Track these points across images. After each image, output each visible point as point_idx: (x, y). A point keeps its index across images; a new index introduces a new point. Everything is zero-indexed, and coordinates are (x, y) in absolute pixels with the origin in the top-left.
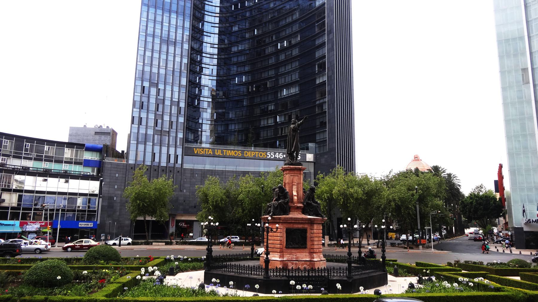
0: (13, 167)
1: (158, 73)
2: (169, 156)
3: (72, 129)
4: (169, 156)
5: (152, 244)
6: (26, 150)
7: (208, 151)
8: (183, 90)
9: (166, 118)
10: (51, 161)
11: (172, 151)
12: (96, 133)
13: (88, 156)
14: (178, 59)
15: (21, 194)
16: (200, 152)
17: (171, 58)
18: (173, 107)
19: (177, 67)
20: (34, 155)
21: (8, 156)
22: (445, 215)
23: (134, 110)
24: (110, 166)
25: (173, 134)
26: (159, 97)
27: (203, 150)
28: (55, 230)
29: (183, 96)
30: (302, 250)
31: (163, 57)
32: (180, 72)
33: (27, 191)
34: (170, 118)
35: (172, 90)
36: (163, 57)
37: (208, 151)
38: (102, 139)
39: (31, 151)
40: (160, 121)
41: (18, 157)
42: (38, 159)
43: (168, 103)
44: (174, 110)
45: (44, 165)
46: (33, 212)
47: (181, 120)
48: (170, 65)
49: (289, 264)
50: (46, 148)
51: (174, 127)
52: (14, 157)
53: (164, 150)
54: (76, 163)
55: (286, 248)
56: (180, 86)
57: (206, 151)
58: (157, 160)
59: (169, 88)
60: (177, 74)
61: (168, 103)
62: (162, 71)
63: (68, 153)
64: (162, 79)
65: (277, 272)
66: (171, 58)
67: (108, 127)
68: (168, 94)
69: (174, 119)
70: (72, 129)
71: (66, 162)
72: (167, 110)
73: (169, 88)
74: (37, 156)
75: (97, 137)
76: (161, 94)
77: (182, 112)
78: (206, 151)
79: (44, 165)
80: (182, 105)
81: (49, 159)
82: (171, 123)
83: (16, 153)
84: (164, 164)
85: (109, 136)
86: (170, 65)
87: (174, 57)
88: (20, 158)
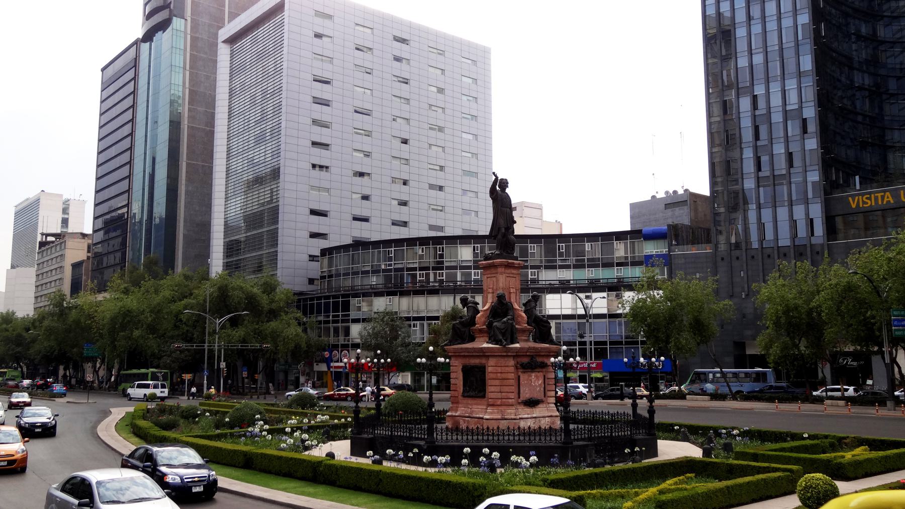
0: (548, 283)
1: (751, 66)
2: (793, 224)
3: (633, 206)
4: (793, 224)
5: (685, 398)
6: (561, 255)
7: (883, 197)
8: (809, 84)
9: (779, 149)
10: (597, 266)
11: (799, 212)
12: (667, 206)
13: (651, 248)
14: (787, 22)
15: (558, 321)
16: (864, 202)
17: (772, 26)
18: (789, 123)
19: (788, 38)
20: (572, 260)
21: (538, 267)
22: (777, 324)
23: (715, 150)
24: (683, 261)
25: (796, 179)
26: (757, 112)
27: (869, 199)
28: (211, 364)
29: (810, 94)
30: (478, 401)
31: (757, 29)
32: (797, 45)
33: (566, 317)
34: (787, 148)
35: (784, 92)
36: (757, 29)
37: (883, 197)
38: (677, 213)
39: (568, 254)
40: (765, 159)
41: (551, 267)
42: (579, 266)
43: (777, 118)
44: (794, 129)
45: (588, 274)
46: (577, 347)
47: (812, 143)
48: (773, 40)
49: (461, 422)
50: (588, 246)
51: (797, 162)
52: (547, 267)
53: (783, 213)
54: (635, 264)
55: (463, 396)
56: (800, 74)
57: (876, 198)
58: (769, 235)
59: (775, 88)
60: (789, 54)
61: (777, 118)
62: (758, 59)
63: (620, 250)
64: (759, 74)
65: (478, 435)
66: (772, 26)
67: (667, 192)
68: (776, 100)
69: (794, 148)
70: (633, 206)
71: (619, 264)
72: (779, 132)
73: (775, 88)
74: (577, 260)
75: (669, 212)
76: (762, 104)
77: (812, 127)
78: (876, 198)
79: (588, 274)
80: (810, 112)
81: (593, 264)
82: (790, 156)
83: (548, 261)
84: (785, 241)
85: (686, 207)
86: (773, 40)
87: (779, 19)
88: (554, 267)
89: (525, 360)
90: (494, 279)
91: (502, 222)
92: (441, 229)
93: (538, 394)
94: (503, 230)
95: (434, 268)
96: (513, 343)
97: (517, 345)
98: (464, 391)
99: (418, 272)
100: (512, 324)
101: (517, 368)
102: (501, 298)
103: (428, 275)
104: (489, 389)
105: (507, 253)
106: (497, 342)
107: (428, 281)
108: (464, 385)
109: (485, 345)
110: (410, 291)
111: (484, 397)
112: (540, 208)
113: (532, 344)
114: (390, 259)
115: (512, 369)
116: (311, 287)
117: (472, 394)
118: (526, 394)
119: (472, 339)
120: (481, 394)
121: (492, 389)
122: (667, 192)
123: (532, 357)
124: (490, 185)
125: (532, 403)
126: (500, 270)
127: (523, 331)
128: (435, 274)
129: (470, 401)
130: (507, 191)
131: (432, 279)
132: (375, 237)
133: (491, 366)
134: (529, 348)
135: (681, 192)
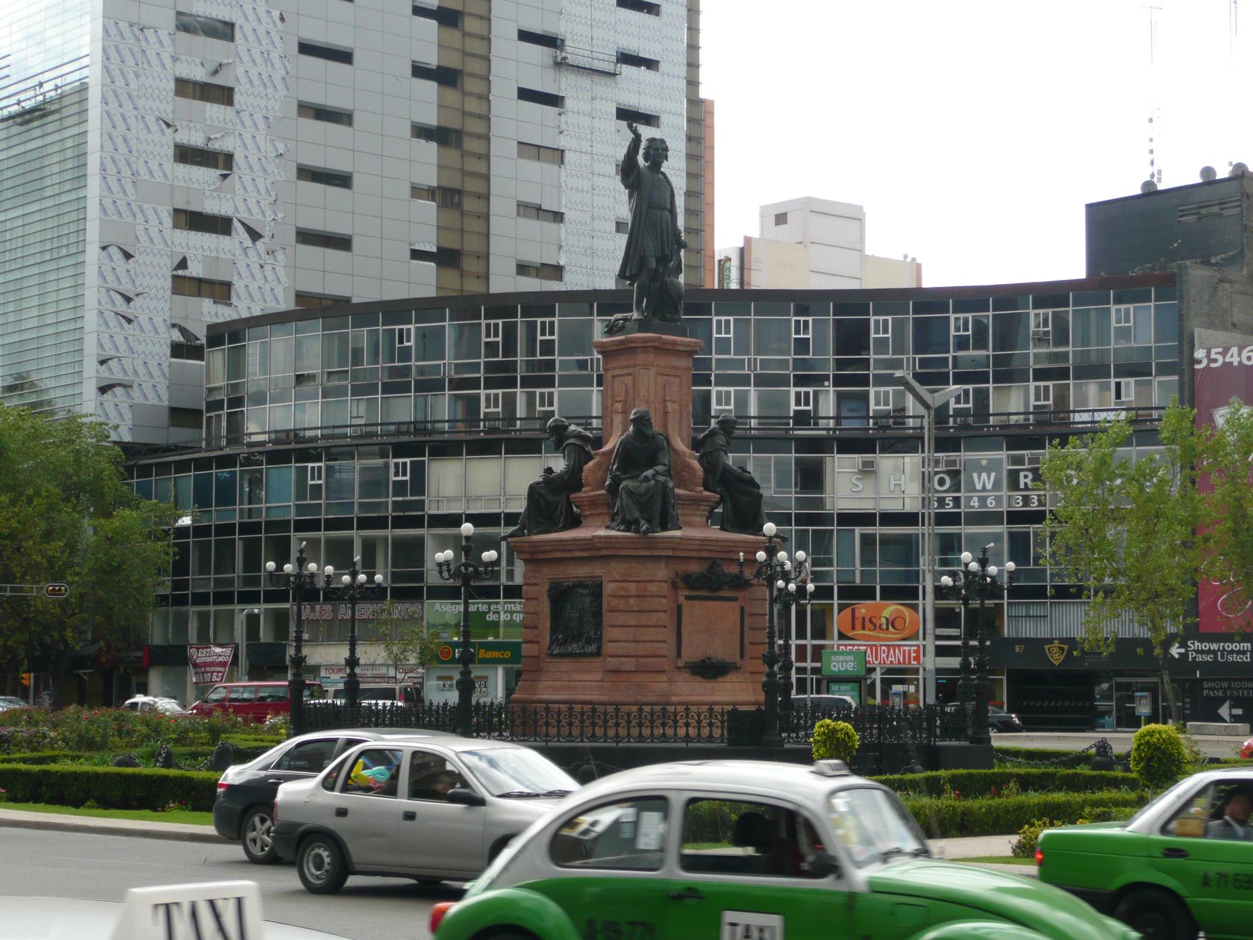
15: (868, 530)
89: (694, 568)
90: (629, 380)
91: (650, 247)
92: (556, 271)
93: (722, 648)
94: (653, 264)
95: (527, 382)
96: (665, 528)
97: (677, 533)
98: (552, 642)
99: (483, 392)
100: (664, 485)
101: (675, 587)
102: (642, 421)
103: (510, 402)
104: (609, 633)
105: (664, 319)
106: (629, 525)
107: (510, 416)
108: (554, 629)
109: (602, 532)
110: (459, 443)
111: (598, 653)
112: (855, 217)
113: (715, 533)
114: (405, 354)
115: (665, 588)
116: (180, 435)
117: (574, 647)
118: (692, 653)
119: (574, 522)
120: (592, 648)
121: (614, 635)
122: (1208, 172)
123: (713, 563)
124: (621, 153)
125: (710, 669)
126: (641, 358)
127: (695, 502)
128: (531, 399)
129: (566, 664)
130: (665, 167)
131: (521, 411)
132: (363, 293)
133: (612, 578)
134: (704, 541)
135: (1223, 172)
